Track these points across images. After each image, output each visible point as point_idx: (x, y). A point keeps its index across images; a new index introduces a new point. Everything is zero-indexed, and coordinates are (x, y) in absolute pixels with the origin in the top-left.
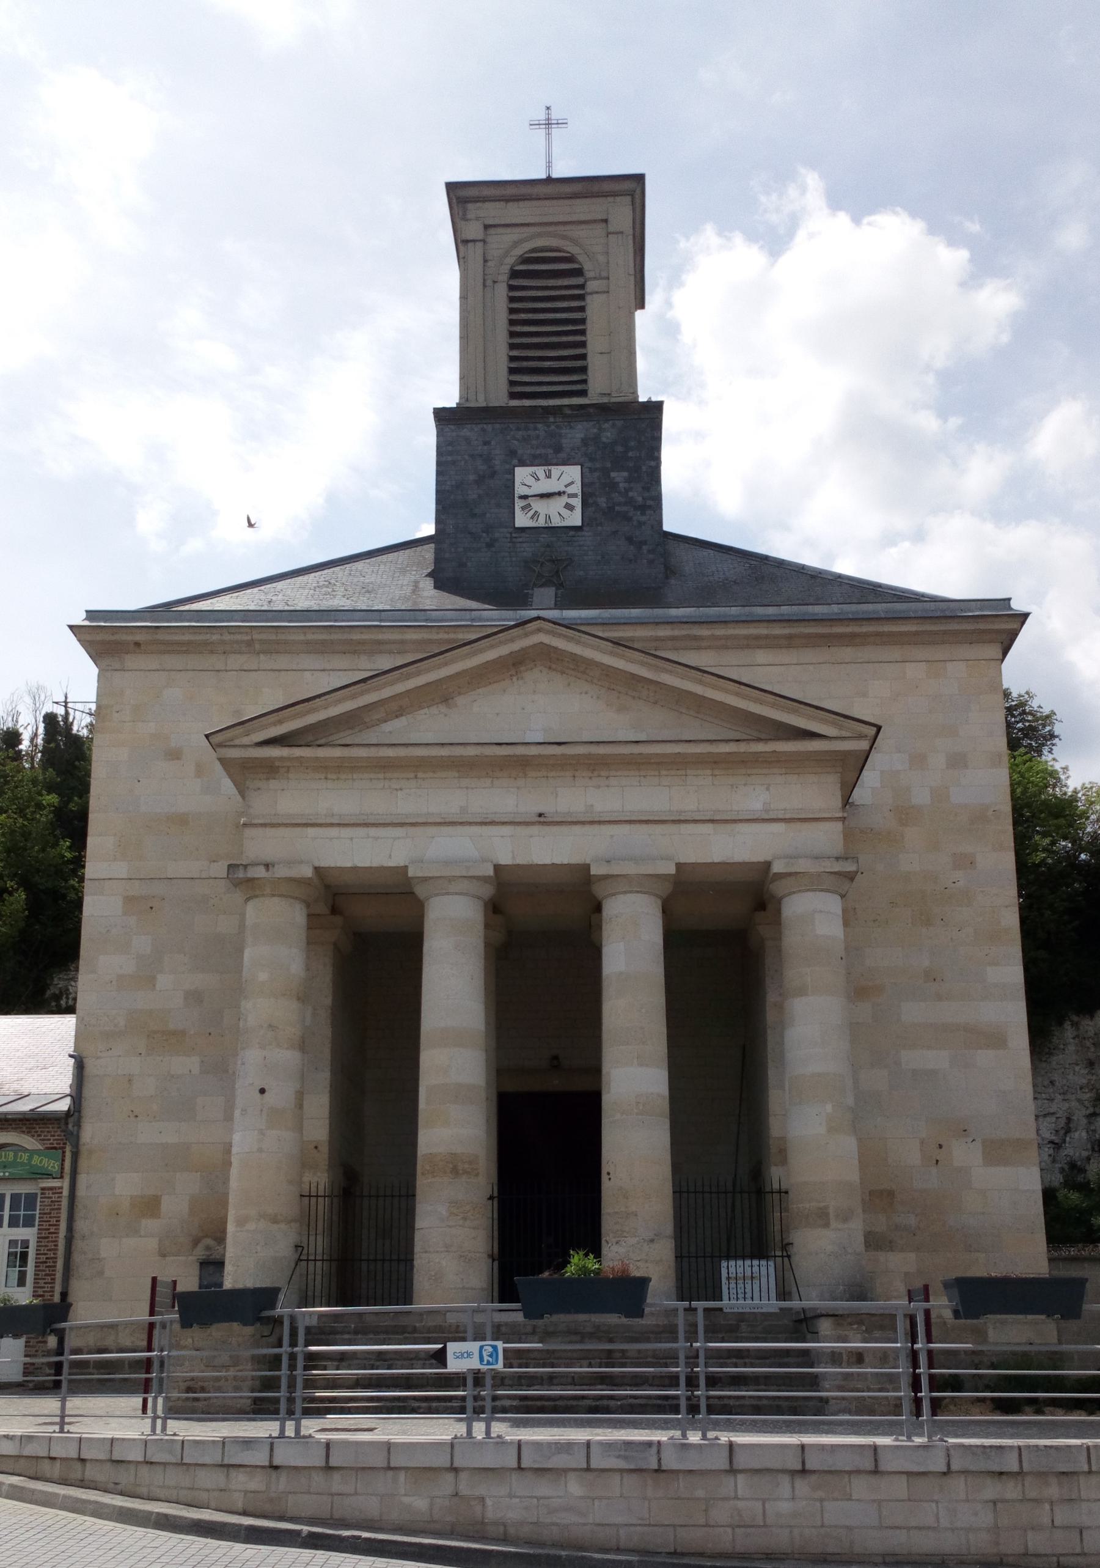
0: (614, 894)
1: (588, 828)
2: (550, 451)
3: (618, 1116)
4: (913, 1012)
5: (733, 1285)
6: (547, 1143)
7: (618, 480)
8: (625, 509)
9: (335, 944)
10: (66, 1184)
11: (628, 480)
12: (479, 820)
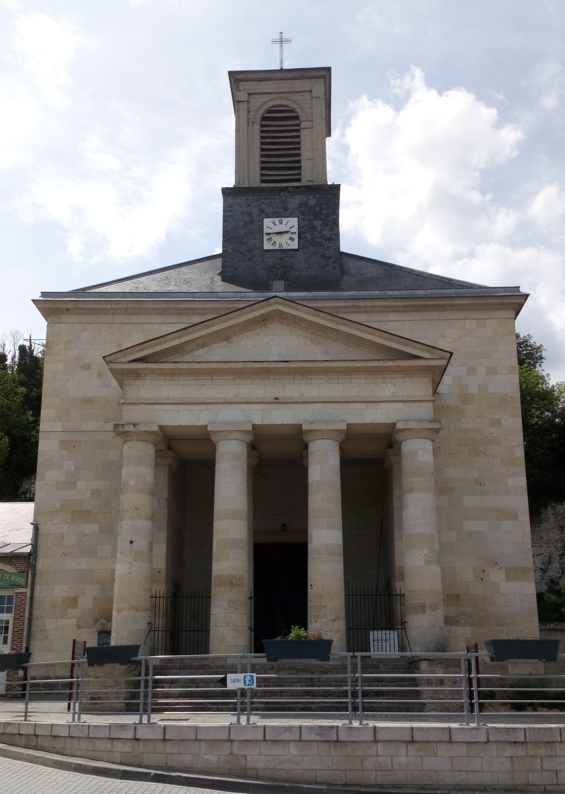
2: (282, 210)
3: (316, 556)
4: (470, 501)
7: (317, 225)
8: (320, 240)
11: (322, 226)
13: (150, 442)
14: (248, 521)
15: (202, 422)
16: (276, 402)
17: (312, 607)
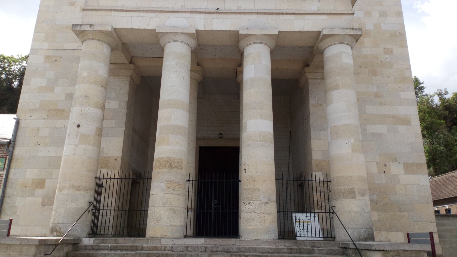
0: (249, 44)
1: (239, 16)
3: (250, 142)
5: (305, 225)
6: (217, 167)
9: (131, 76)
10: (4, 173)
12: (189, 11)
13: (105, 42)
14: (190, 112)
15: (151, 27)
16: (217, 12)
17: (245, 189)
